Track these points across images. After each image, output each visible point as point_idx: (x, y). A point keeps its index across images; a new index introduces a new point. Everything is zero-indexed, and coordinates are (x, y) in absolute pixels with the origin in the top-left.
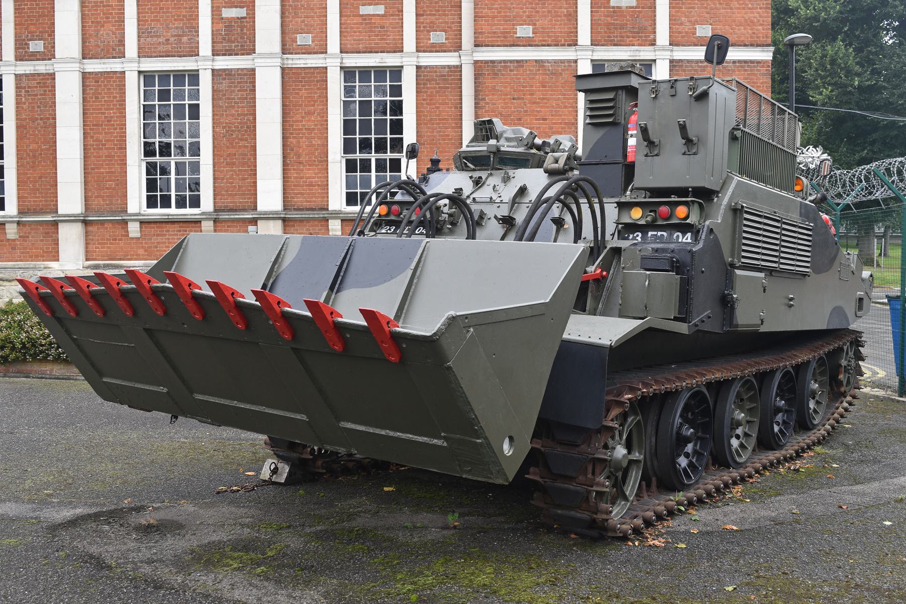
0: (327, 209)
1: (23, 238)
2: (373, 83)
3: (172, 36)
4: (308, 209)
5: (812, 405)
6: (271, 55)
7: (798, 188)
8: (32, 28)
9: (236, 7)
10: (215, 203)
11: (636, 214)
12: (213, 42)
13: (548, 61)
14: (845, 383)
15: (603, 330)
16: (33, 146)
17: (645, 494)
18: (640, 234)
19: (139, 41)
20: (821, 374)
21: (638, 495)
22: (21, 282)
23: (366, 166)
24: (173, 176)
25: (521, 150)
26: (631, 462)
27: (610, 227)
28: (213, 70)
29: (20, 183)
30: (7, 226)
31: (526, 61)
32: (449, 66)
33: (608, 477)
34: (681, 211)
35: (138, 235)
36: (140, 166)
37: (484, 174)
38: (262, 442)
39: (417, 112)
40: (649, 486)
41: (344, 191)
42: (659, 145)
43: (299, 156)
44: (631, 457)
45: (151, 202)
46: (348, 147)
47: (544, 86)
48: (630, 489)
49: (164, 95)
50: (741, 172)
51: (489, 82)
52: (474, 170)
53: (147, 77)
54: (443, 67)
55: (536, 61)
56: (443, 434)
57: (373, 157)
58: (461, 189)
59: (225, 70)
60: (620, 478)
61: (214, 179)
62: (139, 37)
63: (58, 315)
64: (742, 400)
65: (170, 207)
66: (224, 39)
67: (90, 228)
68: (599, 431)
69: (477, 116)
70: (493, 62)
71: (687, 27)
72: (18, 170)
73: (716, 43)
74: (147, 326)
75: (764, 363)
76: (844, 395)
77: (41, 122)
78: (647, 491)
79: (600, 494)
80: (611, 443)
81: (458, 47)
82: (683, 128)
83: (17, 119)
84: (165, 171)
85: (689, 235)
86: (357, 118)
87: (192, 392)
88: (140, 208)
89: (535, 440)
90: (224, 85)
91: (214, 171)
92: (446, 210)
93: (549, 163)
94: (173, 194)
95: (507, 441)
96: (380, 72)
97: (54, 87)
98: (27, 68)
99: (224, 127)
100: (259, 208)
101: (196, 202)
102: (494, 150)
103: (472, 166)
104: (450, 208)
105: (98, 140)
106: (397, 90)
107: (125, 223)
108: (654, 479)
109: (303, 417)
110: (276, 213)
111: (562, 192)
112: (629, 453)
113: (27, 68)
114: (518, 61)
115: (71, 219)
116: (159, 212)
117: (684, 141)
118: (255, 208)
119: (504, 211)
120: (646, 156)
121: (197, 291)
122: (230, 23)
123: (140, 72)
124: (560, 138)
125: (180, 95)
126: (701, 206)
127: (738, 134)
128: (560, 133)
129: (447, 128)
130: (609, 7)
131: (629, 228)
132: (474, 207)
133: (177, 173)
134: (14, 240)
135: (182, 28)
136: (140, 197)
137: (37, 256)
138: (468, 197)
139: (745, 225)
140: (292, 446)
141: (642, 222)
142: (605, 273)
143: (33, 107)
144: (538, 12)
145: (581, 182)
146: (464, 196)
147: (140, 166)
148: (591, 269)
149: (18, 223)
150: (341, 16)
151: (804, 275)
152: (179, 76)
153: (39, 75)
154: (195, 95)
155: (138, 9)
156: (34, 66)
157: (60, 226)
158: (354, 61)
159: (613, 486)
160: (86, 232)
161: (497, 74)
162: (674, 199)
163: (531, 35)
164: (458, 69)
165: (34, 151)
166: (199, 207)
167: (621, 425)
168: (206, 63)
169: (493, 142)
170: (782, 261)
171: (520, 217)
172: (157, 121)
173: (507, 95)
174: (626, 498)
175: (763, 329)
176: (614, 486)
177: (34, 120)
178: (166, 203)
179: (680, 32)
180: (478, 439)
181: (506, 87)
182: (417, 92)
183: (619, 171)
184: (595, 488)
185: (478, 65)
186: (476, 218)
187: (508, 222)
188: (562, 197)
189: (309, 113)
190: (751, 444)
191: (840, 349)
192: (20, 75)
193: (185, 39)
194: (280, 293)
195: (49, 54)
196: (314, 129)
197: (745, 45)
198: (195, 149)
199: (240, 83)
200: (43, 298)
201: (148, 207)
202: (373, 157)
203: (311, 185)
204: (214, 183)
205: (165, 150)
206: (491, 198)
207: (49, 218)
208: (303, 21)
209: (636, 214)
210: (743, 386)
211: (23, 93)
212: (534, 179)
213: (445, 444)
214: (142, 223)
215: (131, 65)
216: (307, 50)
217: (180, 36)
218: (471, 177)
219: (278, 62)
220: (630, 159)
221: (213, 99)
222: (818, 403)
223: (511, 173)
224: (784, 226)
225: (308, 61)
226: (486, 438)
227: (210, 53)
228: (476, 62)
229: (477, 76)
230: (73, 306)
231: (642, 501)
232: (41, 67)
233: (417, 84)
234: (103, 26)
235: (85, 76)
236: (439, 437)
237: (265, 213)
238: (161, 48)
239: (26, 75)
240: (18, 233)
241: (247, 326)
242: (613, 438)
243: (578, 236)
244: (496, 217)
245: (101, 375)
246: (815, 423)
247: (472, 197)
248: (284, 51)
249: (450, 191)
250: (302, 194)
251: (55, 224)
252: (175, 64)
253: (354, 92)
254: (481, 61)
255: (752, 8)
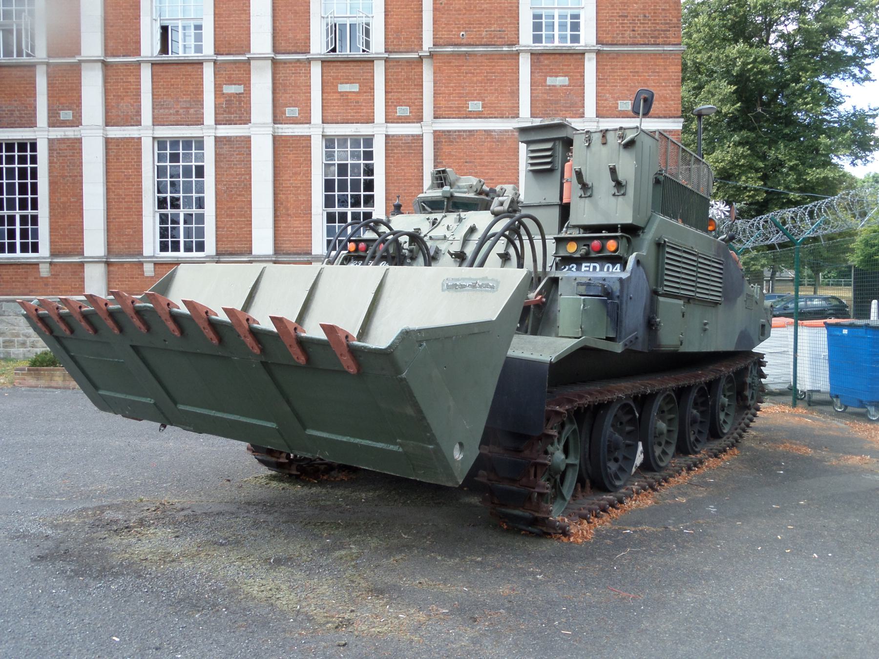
0: (311, 254)
1: (55, 275)
2: (349, 149)
3: (182, 108)
4: (295, 254)
5: (722, 416)
6: (264, 125)
7: (710, 228)
8: (63, 100)
9: (235, 84)
10: (217, 248)
11: (572, 248)
12: (216, 114)
13: (494, 131)
14: (749, 398)
15: (543, 349)
16: (63, 199)
17: (580, 495)
18: (575, 266)
19: (153, 112)
20: (729, 389)
21: (574, 496)
22: (22, 304)
23: (343, 217)
24: (182, 225)
25: (472, 195)
26: (568, 466)
27: (550, 260)
28: (216, 137)
29: (53, 230)
30: (41, 266)
31: (477, 131)
32: (413, 136)
33: (548, 480)
34: (611, 245)
35: (152, 274)
36: (154, 217)
37: (438, 216)
38: (245, 449)
39: (386, 173)
40: (583, 486)
41: (325, 238)
42: (591, 188)
43: (287, 210)
44: (569, 461)
45: (164, 247)
46: (329, 202)
47: (491, 152)
48: (567, 490)
49: (175, 158)
50: (665, 213)
51: (446, 149)
52: (431, 213)
53: (161, 143)
54: (408, 136)
55: (485, 131)
56: (398, 440)
57: (18, 213)
58: (419, 229)
59: (225, 137)
60: (558, 480)
61: (217, 228)
62: (153, 108)
63: (55, 334)
64: (663, 412)
65: (179, 251)
66: (225, 111)
67: (111, 268)
68: (540, 439)
69: (435, 167)
70: (449, 131)
71: (611, 103)
72: (50, 219)
73: (642, 97)
74: (134, 344)
75: (683, 379)
76: (749, 408)
77: (70, 179)
78: (582, 492)
79: (541, 495)
80: (550, 449)
81: (420, 119)
82: (613, 171)
83: (50, 176)
84: (175, 221)
85: (618, 266)
86: (336, 178)
87: (175, 403)
88: (154, 252)
89: (483, 446)
90: (225, 149)
91: (216, 221)
92: (406, 246)
93: (495, 207)
94: (182, 240)
95: (457, 446)
96: (355, 141)
97: (81, 149)
98: (58, 133)
99: (225, 185)
100: (254, 253)
101: (35, 248)
102: (448, 195)
103: (429, 210)
104: (410, 245)
105: (118, 195)
106: (369, 155)
107: (141, 264)
108: (588, 481)
109: (274, 425)
110: (268, 256)
111: (507, 228)
112: (567, 457)
113: (58, 133)
114: (470, 131)
115: (95, 261)
116: (170, 254)
117: (614, 184)
118: (251, 253)
119: (456, 248)
120: (581, 197)
121: (176, 310)
122: (230, 99)
123: (154, 138)
124: (505, 186)
125: (187, 157)
126: (629, 240)
127: (662, 178)
128: (505, 183)
129: (411, 186)
130: (546, 86)
131: (567, 260)
132: (429, 244)
133: (185, 222)
134: (47, 278)
135: (189, 102)
136: (154, 242)
137: (66, 291)
138: (425, 236)
139: (668, 258)
140: (270, 452)
141: (577, 255)
142: (544, 300)
143: (63, 167)
144: (486, 90)
145: (525, 220)
146: (422, 235)
147: (154, 217)
148: (532, 296)
149: (51, 263)
150: (322, 93)
151: (716, 304)
152: (187, 143)
153: (68, 139)
154: (201, 158)
155: (153, 85)
156: (64, 131)
157: (86, 266)
158: (333, 130)
159: (552, 488)
160: (109, 272)
161: (452, 142)
162: (604, 234)
163: (480, 109)
164: (419, 138)
165: (63, 203)
166: (203, 250)
167: (560, 433)
168: (209, 130)
169: (447, 188)
170: (698, 290)
171: (469, 251)
172: (169, 179)
173: (460, 159)
174: (564, 498)
175: (684, 349)
176: (554, 487)
177: (64, 177)
178: (176, 247)
179: (605, 107)
180: (431, 444)
181: (460, 153)
182: (386, 156)
183: (556, 212)
184: (537, 490)
185: (438, 136)
186: (432, 253)
187: (460, 257)
188: (507, 233)
189: (295, 174)
190: (671, 450)
191: (746, 368)
192: (53, 139)
193: (192, 111)
194: (253, 313)
195: (76, 122)
196: (300, 187)
197: (659, 117)
198: (200, 203)
199: (238, 148)
200: (42, 319)
201: (161, 251)
202: (349, 210)
203: (297, 233)
204: (216, 231)
205: (175, 204)
206: (445, 236)
207: (76, 259)
208: (291, 97)
209: (572, 248)
210: (664, 399)
211: (55, 155)
212: (481, 219)
213: (401, 450)
214: (155, 264)
215: (146, 132)
216: (294, 121)
217: (188, 108)
218: (428, 219)
219: (270, 131)
220: (565, 201)
221: (216, 161)
222: (727, 414)
223: (463, 214)
224: (700, 260)
225: (295, 130)
226: (437, 444)
227: (213, 122)
228: (435, 132)
229: (436, 143)
230: (68, 325)
231: (578, 501)
232: (70, 133)
233: (386, 150)
234: (123, 99)
235: (108, 141)
236: (396, 444)
237: (259, 256)
238: (172, 118)
239: (58, 140)
240: (51, 272)
241: (221, 340)
242: (552, 444)
243: (520, 265)
244: (449, 252)
245: (96, 388)
246: (725, 431)
247: (429, 235)
248: (276, 121)
249: (411, 230)
250: (290, 241)
251: (82, 264)
252: (184, 132)
253: (334, 156)
254: (439, 131)
255: (666, 86)
